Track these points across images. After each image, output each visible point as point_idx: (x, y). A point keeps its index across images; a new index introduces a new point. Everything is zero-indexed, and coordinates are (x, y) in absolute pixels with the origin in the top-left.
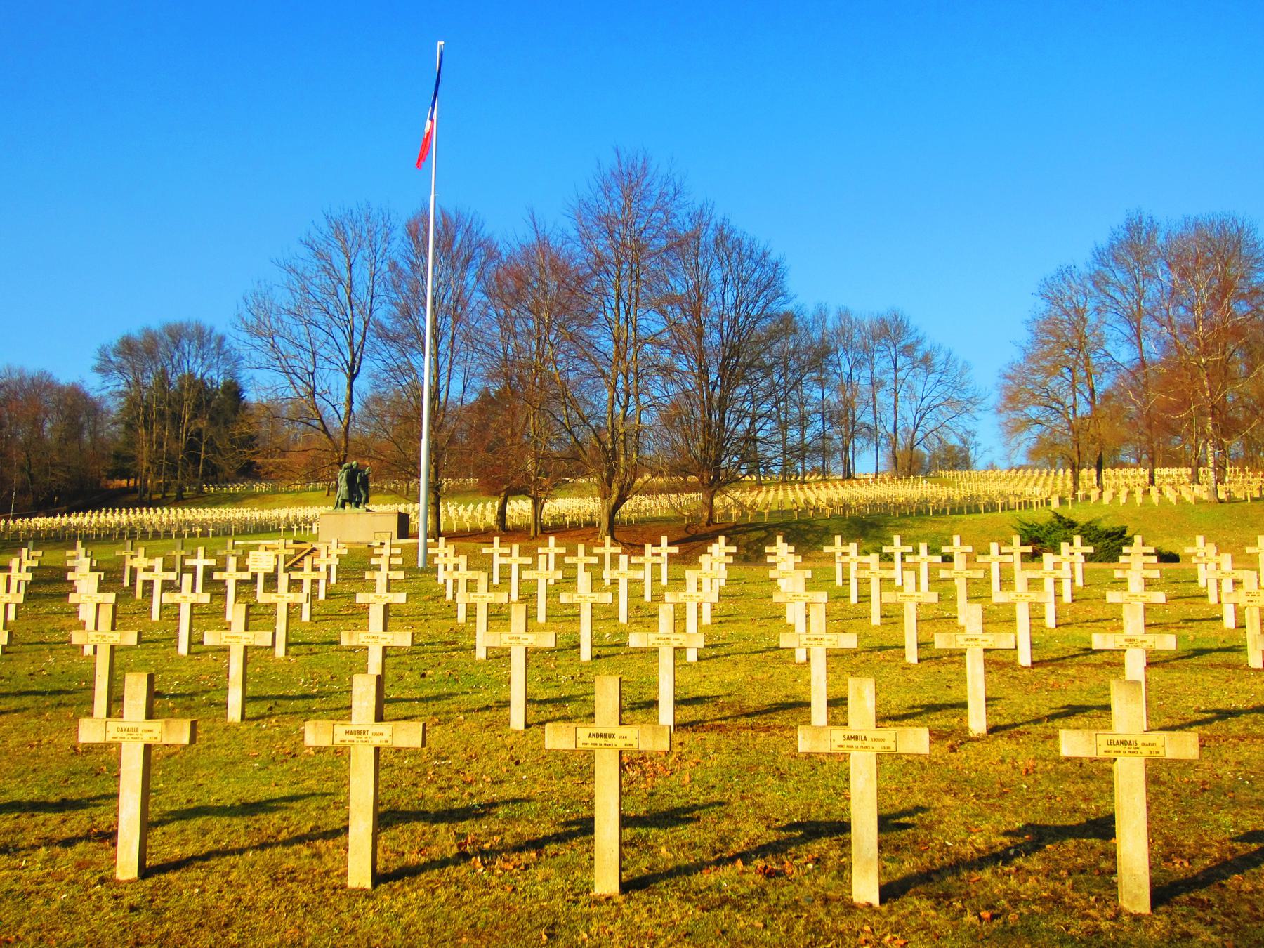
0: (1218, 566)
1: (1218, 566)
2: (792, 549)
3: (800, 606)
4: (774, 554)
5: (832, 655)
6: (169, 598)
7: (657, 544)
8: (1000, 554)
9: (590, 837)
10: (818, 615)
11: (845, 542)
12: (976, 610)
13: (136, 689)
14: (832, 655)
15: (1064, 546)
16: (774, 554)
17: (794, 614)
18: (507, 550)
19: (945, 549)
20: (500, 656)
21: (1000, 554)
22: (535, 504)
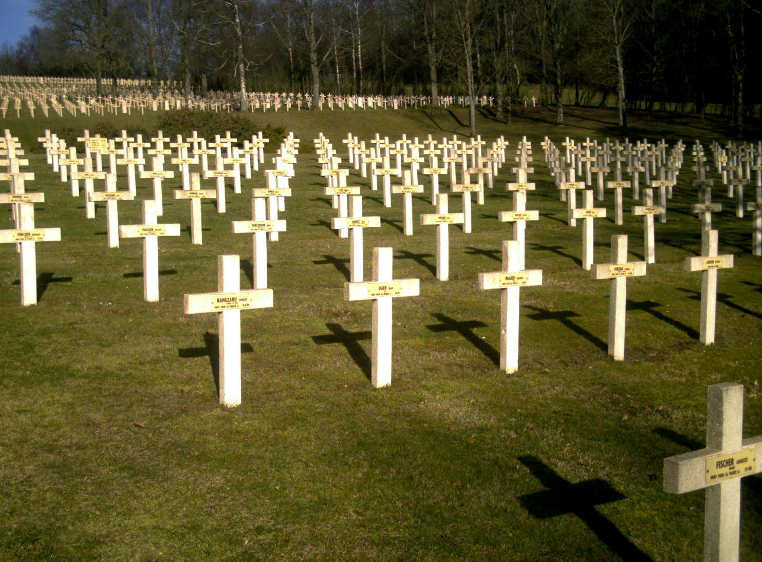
0: (68, 157)
1: (68, 157)
2: (283, 145)
3: (344, 198)
4: (17, 149)
5: (367, 232)
6: (397, 190)
7: (223, 136)
8: (208, 148)
9: (244, 342)
10: (358, 202)
11: (382, 138)
12: (444, 198)
13: (385, 256)
14: (367, 232)
15: (254, 137)
16: (17, 149)
17: (340, 203)
18: (393, 146)
19: (153, 140)
20: (581, 221)
21: (208, 148)
22: (97, 81)
